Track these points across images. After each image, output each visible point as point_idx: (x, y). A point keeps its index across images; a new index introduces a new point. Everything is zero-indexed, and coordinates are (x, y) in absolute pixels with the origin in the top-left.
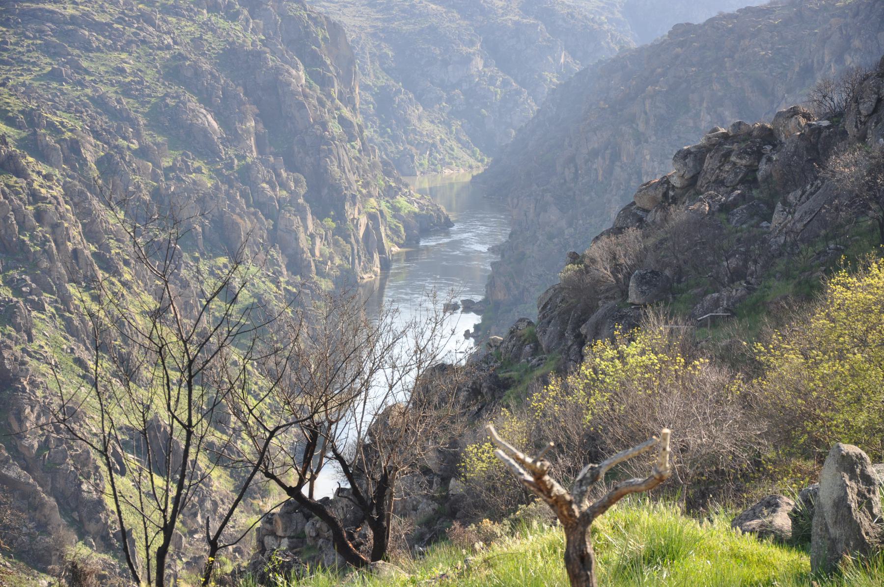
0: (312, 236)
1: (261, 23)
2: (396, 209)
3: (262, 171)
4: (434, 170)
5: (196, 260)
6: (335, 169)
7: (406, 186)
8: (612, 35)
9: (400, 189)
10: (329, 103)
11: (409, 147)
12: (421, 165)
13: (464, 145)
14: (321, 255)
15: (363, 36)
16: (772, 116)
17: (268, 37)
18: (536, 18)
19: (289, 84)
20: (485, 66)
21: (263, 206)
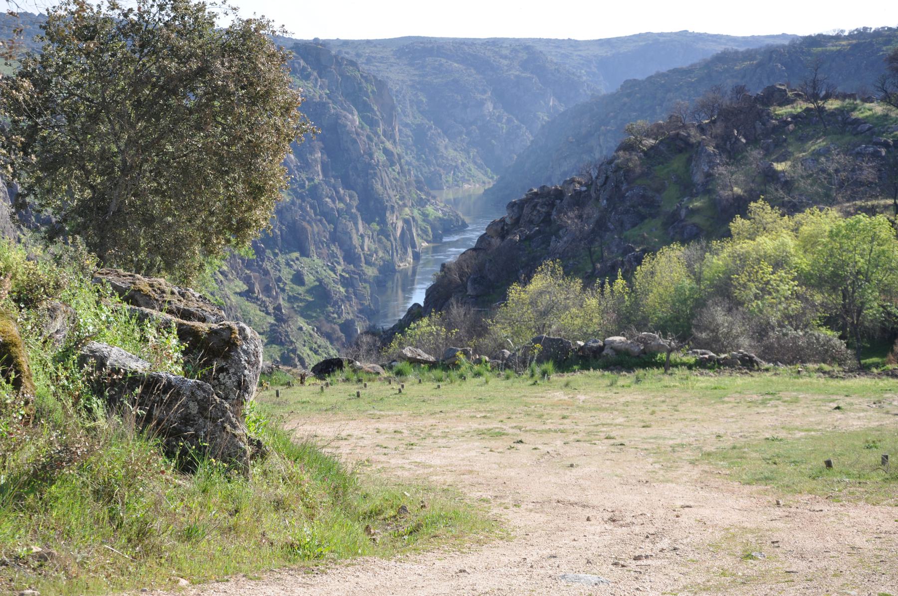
0: (362, 236)
1: (326, 82)
2: (425, 216)
3: (326, 190)
4: (457, 185)
5: (276, 255)
6: (378, 187)
7: (434, 197)
8: (588, 85)
9: (429, 200)
10: (375, 139)
11: (438, 168)
12: (447, 181)
13: (480, 167)
14: (369, 249)
15: (404, 87)
16: (562, 182)
17: (332, 92)
18: (532, 73)
19: (345, 126)
20: (494, 108)
21: (327, 215)
